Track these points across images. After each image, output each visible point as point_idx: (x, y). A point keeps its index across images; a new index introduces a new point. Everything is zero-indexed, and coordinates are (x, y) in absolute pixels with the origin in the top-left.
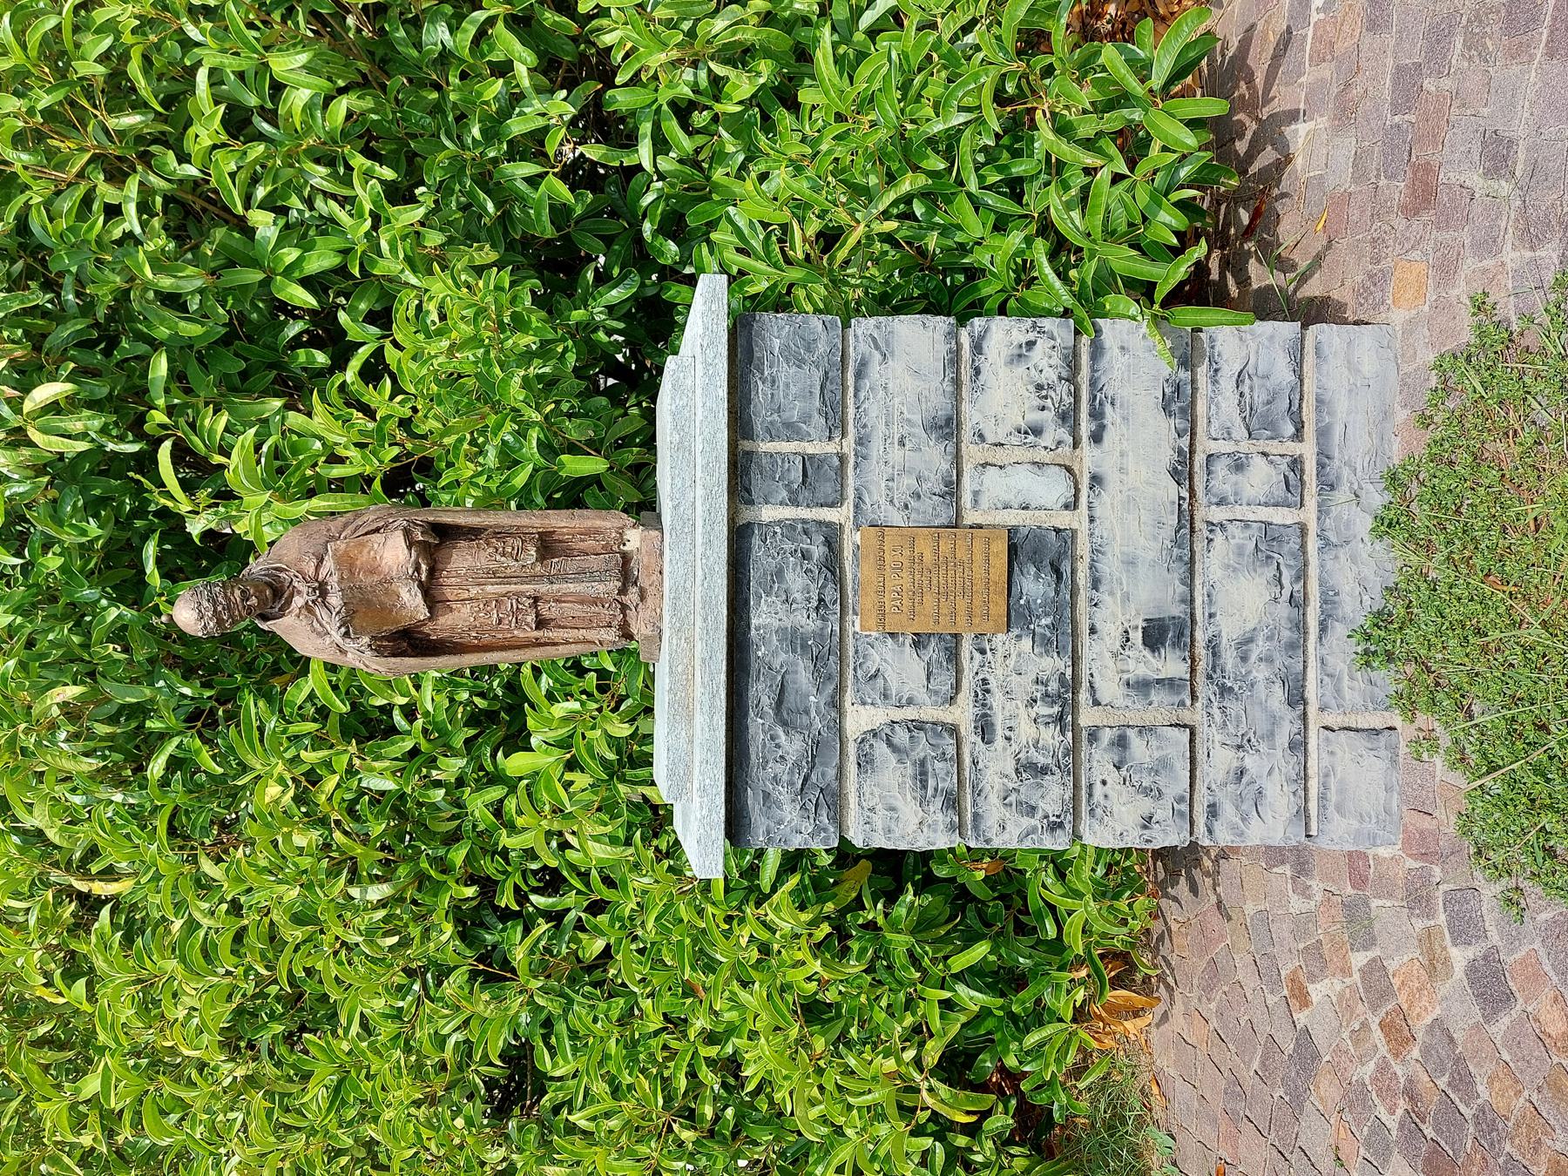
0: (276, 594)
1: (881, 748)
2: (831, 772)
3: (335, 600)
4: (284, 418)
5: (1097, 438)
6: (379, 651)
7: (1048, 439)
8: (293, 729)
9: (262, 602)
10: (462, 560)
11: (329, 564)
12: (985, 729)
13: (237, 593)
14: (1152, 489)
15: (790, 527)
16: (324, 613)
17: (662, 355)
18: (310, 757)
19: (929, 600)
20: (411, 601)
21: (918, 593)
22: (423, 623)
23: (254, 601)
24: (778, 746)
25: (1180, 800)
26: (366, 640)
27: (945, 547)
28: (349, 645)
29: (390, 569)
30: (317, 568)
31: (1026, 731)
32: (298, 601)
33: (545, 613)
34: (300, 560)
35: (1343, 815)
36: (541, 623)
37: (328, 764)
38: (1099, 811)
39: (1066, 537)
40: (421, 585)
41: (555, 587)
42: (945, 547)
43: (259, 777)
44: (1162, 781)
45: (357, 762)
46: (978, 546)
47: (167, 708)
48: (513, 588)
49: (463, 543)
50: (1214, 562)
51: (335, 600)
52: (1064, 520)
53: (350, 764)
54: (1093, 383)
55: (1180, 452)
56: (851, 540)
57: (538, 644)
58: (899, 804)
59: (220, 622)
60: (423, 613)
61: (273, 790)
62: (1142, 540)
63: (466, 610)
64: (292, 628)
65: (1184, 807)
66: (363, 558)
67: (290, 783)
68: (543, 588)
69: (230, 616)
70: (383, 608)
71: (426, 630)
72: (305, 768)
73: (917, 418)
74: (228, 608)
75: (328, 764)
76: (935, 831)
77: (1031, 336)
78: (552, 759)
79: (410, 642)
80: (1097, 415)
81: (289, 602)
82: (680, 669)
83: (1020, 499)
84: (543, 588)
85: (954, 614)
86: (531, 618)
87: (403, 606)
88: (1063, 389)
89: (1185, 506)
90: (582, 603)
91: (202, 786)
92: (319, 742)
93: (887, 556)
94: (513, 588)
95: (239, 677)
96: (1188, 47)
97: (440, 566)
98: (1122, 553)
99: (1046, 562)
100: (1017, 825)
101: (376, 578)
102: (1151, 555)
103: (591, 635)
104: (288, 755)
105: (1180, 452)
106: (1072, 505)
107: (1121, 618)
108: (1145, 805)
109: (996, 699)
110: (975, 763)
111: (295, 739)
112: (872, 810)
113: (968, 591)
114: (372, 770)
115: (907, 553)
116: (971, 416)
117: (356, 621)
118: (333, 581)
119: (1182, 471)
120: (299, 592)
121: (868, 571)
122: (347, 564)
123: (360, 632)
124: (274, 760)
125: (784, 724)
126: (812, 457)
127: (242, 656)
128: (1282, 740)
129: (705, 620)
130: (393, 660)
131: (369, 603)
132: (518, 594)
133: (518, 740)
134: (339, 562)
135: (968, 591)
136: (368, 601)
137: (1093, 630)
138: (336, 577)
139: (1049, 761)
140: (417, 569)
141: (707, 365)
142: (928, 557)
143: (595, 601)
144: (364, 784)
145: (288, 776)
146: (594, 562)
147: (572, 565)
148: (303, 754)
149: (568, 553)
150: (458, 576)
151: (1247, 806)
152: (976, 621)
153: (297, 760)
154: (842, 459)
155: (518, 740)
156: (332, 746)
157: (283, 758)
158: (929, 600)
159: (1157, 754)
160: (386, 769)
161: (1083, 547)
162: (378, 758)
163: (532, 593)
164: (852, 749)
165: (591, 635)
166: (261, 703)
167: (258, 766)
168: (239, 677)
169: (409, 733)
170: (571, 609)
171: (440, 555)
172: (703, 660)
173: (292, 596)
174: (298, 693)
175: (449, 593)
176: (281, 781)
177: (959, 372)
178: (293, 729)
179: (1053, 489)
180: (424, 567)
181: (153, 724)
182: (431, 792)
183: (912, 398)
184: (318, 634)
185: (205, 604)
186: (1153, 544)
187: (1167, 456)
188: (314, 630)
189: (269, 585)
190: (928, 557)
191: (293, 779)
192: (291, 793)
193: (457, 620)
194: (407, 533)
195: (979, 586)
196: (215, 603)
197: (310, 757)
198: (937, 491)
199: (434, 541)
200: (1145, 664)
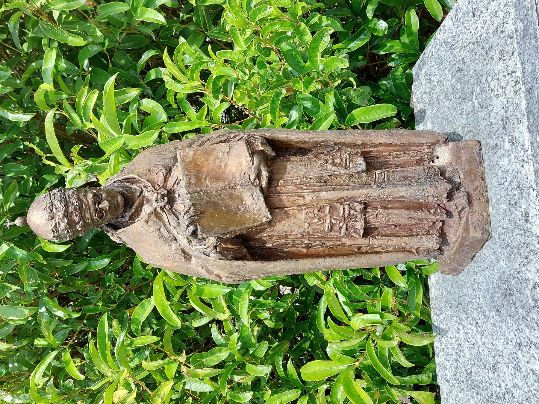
0: (126, 204)
4: (139, 105)
6: (224, 254)
8: (139, 341)
9: (113, 207)
10: (296, 171)
11: (178, 172)
13: (90, 196)
16: (172, 218)
17: (383, 77)
18: (150, 366)
20: (254, 205)
22: (262, 227)
23: (105, 205)
26: (212, 241)
28: (195, 248)
29: (234, 176)
30: (166, 178)
32: (147, 209)
33: (373, 221)
34: (150, 171)
36: (368, 232)
37: (161, 371)
40: (262, 190)
43: (109, 382)
45: (184, 369)
47: (48, 329)
48: (345, 193)
49: (294, 158)
53: (179, 372)
57: (360, 252)
59: (71, 224)
60: (265, 216)
61: (122, 392)
63: (302, 216)
64: (140, 237)
66: (209, 165)
67: (133, 386)
69: (82, 218)
70: (228, 211)
71: (264, 236)
72: (144, 374)
74: (80, 209)
75: (161, 371)
78: (343, 367)
79: (247, 246)
81: (138, 212)
86: (360, 225)
87: (246, 210)
90: (408, 208)
91: (70, 389)
92: (158, 353)
95: (100, 304)
97: (277, 176)
101: (221, 184)
103: (412, 242)
104: (133, 365)
111: (138, 350)
114: (195, 376)
117: (204, 221)
118: (181, 191)
120: (148, 201)
122: (195, 171)
123: (208, 230)
124: (122, 368)
127: (104, 292)
130: (236, 263)
131: (215, 205)
132: (351, 200)
133: (318, 350)
134: (187, 168)
136: (214, 203)
138: (183, 183)
140: (258, 176)
144: (187, 387)
145: (131, 381)
147: (396, 175)
148: (144, 363)
149: (385, 165)
150: (294, 184)
153: (138, 368)
155: (318, 350)
156: (166, 356)
157: (128, 366)
160: (206, 376)
162: (201, 366)
163: (363, 198)
165: (412, 242)
166: (115, 323)
167: (109, 374)
168: (100, 304)
169: (225, 345)
171: (279, 164)
173: (141, 205)
174: (142, 312)
175: (286, 199)
176: (127, 385)
178: (139, 341)
180: (265, 174)
181: (39, 342)
182: (241, 395)
184: (165, 240)
185: (57, 204)
188: (161, 237)
189: (122, 194)
191: (137, 385)
192: (134, 395)
193: (293, 226)
194: (249, 144)
196: (67, 204)
197: (150, 366)
199: (271, 152)
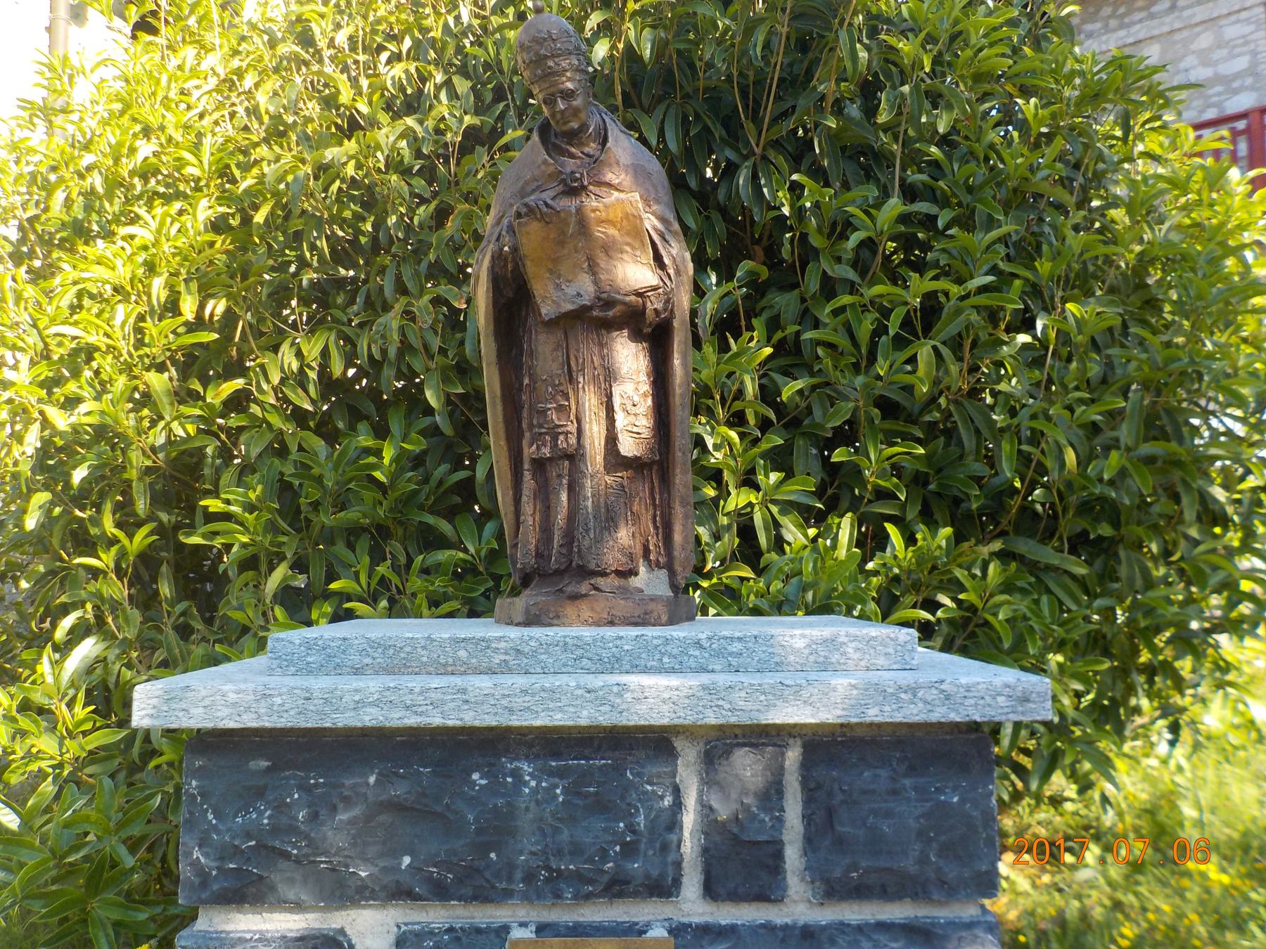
82: (462, 654)
129: (525, 692)
141: (913, 690)
172: (464, 691)
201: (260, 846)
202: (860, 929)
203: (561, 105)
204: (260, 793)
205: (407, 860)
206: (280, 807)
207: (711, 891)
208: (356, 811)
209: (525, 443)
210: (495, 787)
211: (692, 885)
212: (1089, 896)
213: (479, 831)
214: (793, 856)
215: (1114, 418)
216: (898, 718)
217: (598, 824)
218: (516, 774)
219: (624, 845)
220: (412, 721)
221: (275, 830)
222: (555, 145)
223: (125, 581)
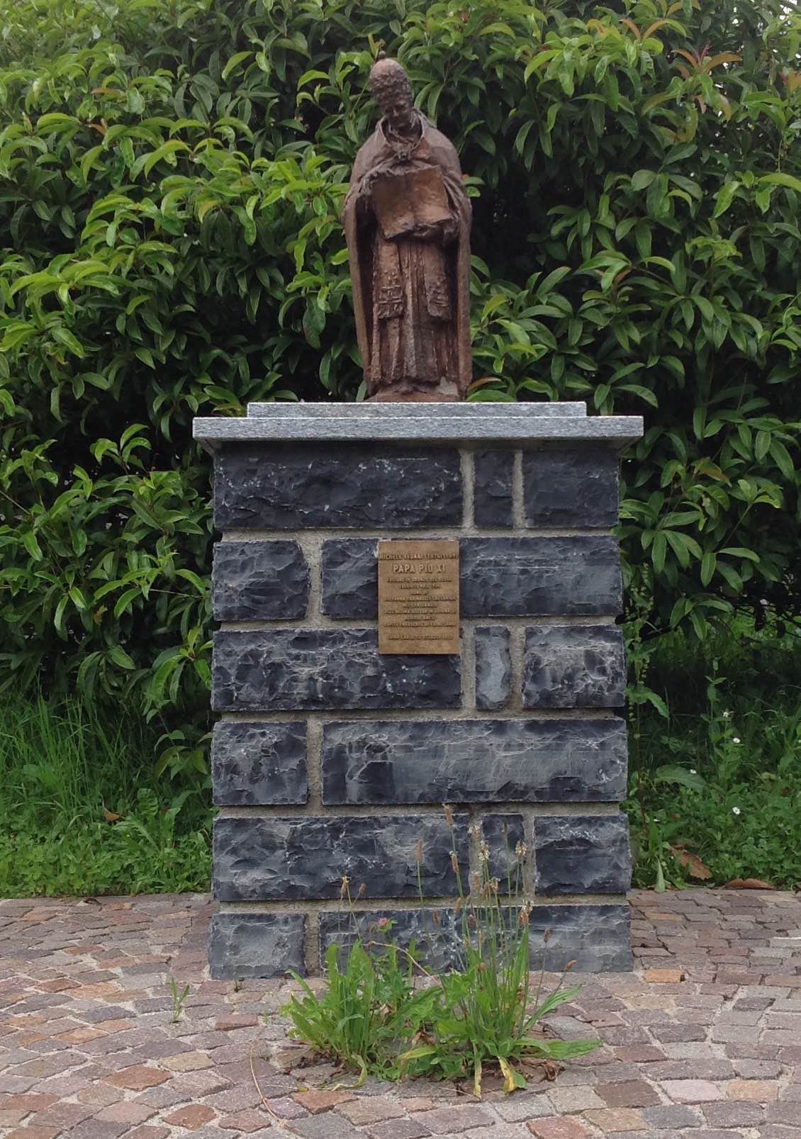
1: (289, 560)
2: (271, 521)
3: (399, 172)
5: (532, 726)
7: (530, 687)
10: (430, 264)
12: (304, 640)
14: (493, 769)
15: (456, 488)
19: (405, 594)
20: (401, 223)
21: (407, 584)
24: (291, 479)
25: (250, 796)
27: (445, 606)
31: (305, 671)
35: (236, 931)
36: (383, 322)
38: (241, 732)
39: (454, 703)
41: (411, 330)
42: (445, 606)
44: (264, 783)
46: (444, 631)
48: (410, 300)
50: (440, 820)
51: (399, 172)
52: (469, 702)
54: (574, 723)
55: (524, 793)
56: (449, 537)
58: (247, 573)
62: (453, 762)
65: (244, 801)
68: (410, 321)
71: (378, 238)
73: (543, 584)
76: (227, 601)
77: (609, 671)
80: (549, 727)
83: (484, 666)
84: (410, 321)
85: (393, 613)
88: (570, 697)
89: (482, 799)
93: (437, 561)
94: (410, 300)
96: (618, 273)
98: (443, 746)
99: (434, 687)
100: (231, 666)
102: (442, 769)
105: (524, 793)
106: (481, 706)
107: (392, 745)
108: (246, 769)
109: (327, 650)
110: (278, 633)
112: (243, 552)
113: (386, 964)
115: (440, 577)
116: (548, 626)
119: (512, 794)
121: (425, 547)
122: (426, 178)
125: (307, 485)
126: (511, 504)
128: (297, 881)
132: (405, 304)
135: (413, 622)
137: (383, 725)
139: (280, 691)
140: (424, 229)
142: (438, 593)
143: (401, 362)
146: (431, 361)
151: (245, 853)
152: (389, 630)
154: (510, 527)
158: (405, 594)
159: (285, 777)
161: (448, 717)
164: (288, 538)
170: (395, 342)
177: (577, 612)
179: (494, 691)
183: (558, 580)
186: (451, 770)
187: (521, 780)
188: (376, 157)
190: (438, 593)
194: (448, 221)
195: (414, 632)
198: (489, 600)
200: (357, 762)
201: (255, 498)
202: (550, 539)
203: (396, 114)
204: (254, 472)
205: (327, 507)
206: (265, 478)
207: (479, 522)
208: (302, 481)
209: (375, 309)
210: (371, 469)
211: (468, 522)
212: (537, 20)
213: (363, 491)
214: (519, 506)
215: (637, 209)
216: (568, 434)
217: (421, 487)
218: (381, 464)
219: (435, 498)
220: (330, 435)
221: (263, 489)
222: (391, 135)
223: (380, 168)
